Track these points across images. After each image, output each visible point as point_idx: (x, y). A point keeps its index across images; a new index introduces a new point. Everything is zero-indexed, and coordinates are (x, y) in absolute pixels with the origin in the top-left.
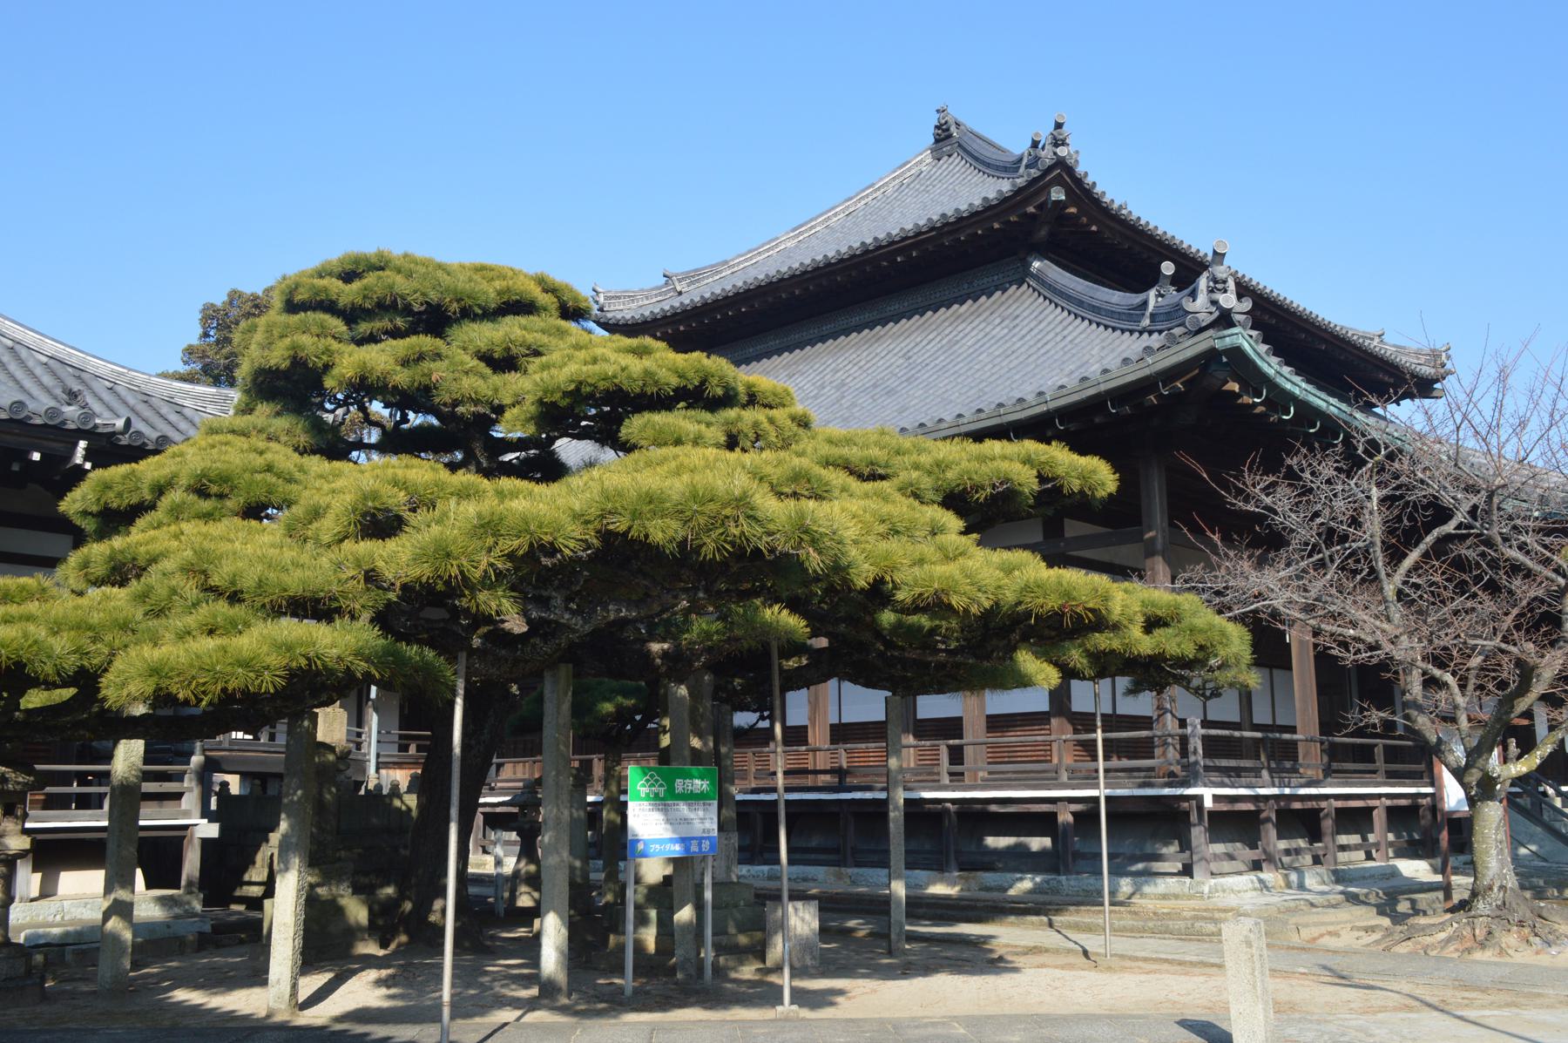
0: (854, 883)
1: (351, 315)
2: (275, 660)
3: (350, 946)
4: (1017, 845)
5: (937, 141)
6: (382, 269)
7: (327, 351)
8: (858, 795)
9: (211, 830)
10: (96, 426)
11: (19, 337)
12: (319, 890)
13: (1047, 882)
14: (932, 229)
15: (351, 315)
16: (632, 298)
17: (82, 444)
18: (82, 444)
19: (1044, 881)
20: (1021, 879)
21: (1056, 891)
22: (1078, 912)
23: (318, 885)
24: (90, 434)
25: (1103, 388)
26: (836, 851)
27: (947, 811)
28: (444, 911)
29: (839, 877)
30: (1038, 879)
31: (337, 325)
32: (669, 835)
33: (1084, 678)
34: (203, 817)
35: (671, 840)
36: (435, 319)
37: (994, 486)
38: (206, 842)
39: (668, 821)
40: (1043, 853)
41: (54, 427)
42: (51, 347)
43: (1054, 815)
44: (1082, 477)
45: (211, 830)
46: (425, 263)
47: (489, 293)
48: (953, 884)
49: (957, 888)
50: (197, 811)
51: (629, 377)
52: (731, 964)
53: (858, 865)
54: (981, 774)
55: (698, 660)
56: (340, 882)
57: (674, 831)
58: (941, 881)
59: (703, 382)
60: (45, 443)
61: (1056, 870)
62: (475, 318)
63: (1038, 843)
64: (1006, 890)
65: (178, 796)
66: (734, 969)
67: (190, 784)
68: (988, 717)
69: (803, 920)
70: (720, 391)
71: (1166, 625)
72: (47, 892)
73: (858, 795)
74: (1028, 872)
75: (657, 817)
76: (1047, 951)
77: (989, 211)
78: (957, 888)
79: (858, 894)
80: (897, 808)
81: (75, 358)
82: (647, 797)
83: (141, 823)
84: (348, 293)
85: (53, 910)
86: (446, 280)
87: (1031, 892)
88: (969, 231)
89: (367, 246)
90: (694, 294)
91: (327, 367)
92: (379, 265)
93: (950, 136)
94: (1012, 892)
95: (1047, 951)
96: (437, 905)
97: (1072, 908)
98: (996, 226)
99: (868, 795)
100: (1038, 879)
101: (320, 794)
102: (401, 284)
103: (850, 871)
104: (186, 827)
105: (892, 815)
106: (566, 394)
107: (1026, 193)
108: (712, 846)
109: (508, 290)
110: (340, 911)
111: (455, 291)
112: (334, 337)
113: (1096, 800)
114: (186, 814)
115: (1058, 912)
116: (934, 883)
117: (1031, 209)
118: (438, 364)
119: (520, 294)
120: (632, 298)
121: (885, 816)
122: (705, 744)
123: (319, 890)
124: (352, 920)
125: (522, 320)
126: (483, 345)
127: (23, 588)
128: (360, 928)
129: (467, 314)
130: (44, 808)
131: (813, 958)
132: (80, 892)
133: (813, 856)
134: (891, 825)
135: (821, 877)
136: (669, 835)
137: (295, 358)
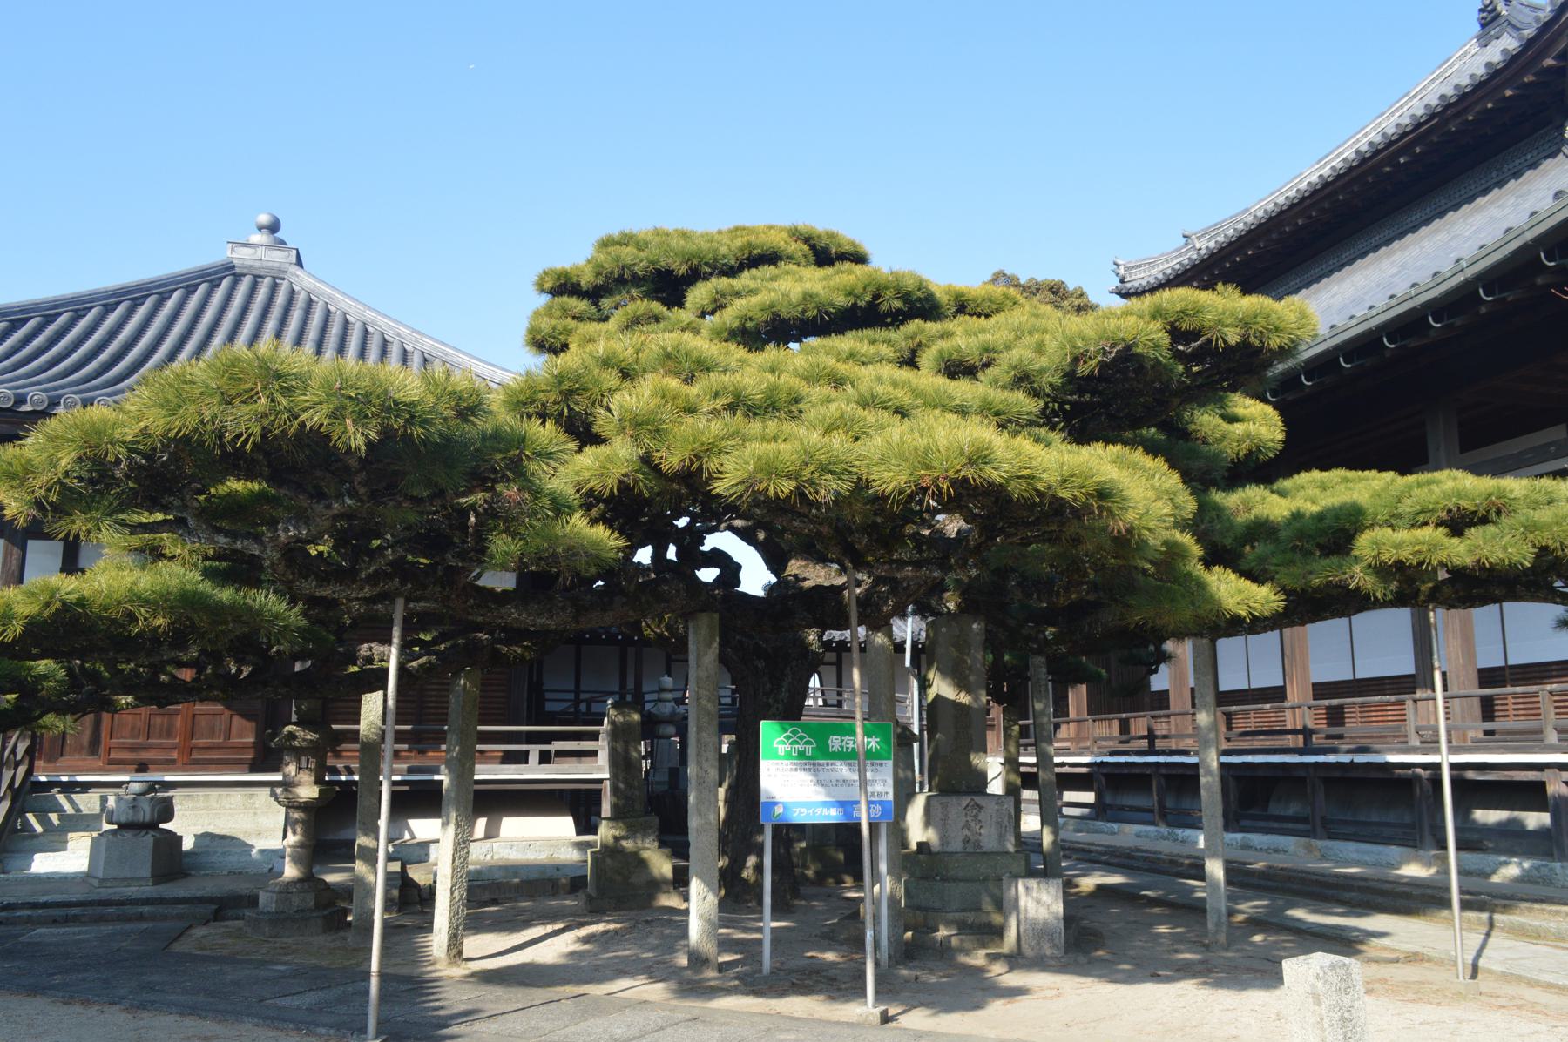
0: (1324, 858)
1: (594, 294)
3: (652, 897)
4: (1510, 821)
5: (1483, 26)
8: (1321, 758)
12: (624, 843)
13: (1538, 869)
14: (1432, 116)
16: (1152, 264)
19: (1534, 868)
20: (1506, 863)
21: (1548, 881)
22: (1530, 910)
25: (1529, 236)
26: (1305, 820)
27: (1418, 777)
28: (759, 868)
29: (1309, 849)
30: (1526, 865)
31: (582, 305)
33: (1377, 604)
35: (825, 804)
36: (668, 285)
37: (1105, 353)
39: (820, 783)
40: (1542, 833)
43: (1541, 786)
44: (1245, 324)
46: (657, 232)
47: (728, 250)
48: (1429, 865)
49: (1433, 870)
52: (967, 945)
53: (1331, 837)
54: (1471, 734)
55: (886, 603)
56: (645, 836)
57: (828, 794)
58: (1416, 859)
59: (876, 296)
61: (1549, 855)
63: (1535, 820)
64: (1488, 876)
65: (594, 753)
66: (967, 952)
67: (603, 746)
68: (1481, 671)
69: (1038, 902)
70: (897, 304)
71: (1484, 521)
72: (491, 834)
73: (1321, 758)
74: (1513, 853)
75: (805, 778)
76: (1430, 960)
77: (1496, 77)
78: (1433, 870)
79: (1345, 876)
80: (1209, 772)
82: (789, 755)
83: (476, 777)
85: (484, 850)
87: (1518, 880)
88: (1478, 108)
90: (1206, 245)
92: (626, 240)
93: (1498, 16)
94: (1495, 879)
95: (1430, 960)
96: (751, 861)
97: (1524, 905)
98: (1508, 93)
99: (1331, 758)
100: (1526, 865)
101: (627, 751)
103: (1319, 843)
105: (1203, 780)
107: (1538, 44)
108: (884, 812)
109: (750, 244)
110: (643, 864)
113: (1436, 767)
115: (1506, 909)
116: (1408, 861)
117: (1549, 62)
120: (1152, 264)
121: (1195, 778)
122: (976, 699)
123: (624, 843)
124: (656, 873)
128: (665, 881)
131: (1056, 946)
133: (1290, 826)
134: (1203, 792)
135: (1291, 849)
136: (823, 798)
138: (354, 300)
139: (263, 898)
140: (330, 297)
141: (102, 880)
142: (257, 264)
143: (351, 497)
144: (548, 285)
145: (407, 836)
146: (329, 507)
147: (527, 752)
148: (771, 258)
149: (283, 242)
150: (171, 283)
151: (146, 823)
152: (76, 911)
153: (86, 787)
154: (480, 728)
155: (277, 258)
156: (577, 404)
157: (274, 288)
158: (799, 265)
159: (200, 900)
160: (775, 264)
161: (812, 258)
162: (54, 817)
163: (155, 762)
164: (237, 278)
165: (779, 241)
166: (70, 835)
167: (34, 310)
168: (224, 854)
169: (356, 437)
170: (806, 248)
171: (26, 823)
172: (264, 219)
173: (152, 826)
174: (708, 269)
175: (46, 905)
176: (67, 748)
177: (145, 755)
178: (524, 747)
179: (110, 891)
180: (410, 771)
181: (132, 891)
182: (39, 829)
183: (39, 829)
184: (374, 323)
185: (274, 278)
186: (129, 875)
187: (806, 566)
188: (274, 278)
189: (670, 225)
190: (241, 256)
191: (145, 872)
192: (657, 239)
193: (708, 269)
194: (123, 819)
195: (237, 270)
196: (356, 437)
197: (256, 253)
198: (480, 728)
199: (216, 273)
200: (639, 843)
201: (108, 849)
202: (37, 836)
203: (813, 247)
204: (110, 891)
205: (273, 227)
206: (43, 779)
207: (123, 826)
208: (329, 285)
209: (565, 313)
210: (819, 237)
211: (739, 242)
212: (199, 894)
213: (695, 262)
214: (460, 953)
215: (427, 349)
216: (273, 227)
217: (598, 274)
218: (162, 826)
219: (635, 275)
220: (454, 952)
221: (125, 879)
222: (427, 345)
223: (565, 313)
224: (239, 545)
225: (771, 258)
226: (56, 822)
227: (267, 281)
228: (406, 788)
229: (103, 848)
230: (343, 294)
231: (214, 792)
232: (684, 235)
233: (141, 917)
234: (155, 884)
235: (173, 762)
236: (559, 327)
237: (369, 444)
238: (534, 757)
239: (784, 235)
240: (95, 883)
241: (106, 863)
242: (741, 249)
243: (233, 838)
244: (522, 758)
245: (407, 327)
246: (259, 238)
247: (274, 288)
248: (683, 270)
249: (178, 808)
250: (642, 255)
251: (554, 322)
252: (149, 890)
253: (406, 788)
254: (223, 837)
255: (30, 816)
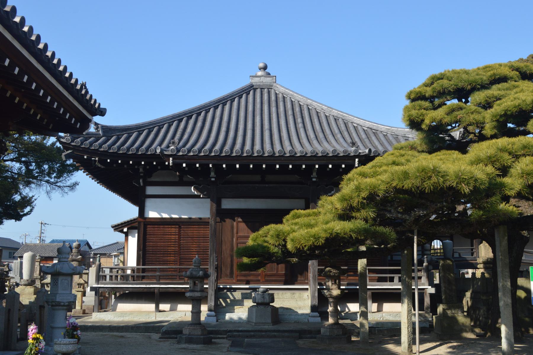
1: (431, 99)
2: (324, 235)
6: (442, 79)
7: (423, 115)
9: (432, 290)
10: (360, 153)
11: (358, 122)
15: (431, 99)
17: (357, 160)
18: (357, 160)
23: (447, 309)
24: (358, 156)
31: (427, 104)
32: (332, 291)
34: (429, 286)
36: (462, 93)
38: (431, 295)
41: (346, 156)
42: (368, 124)
45: (432, 290)
46: (454, 72)
47: (485, 77)
50: (427, 283)
51: (526, 104)
60: (346, 161)
62: (478, 90)
72: (380, 310)
81: (375, 126)
83: (368, 287)
84: (429, 91)
85: (380, 316)
86: (464, 76)
89: (437, 71)
91: (423, 120)
92: (441, 77)
102: (445, 82)
104: (424, 289)
106: (501, 116)
111: (468, 81)
112: (424, 109)
114: (423, 284)
118: (461, 112)
119: (499, 75)
125: (500, 86)
126: (478, 101)
127: (314, 213)
129: (474, 89)
130: (378, 282)
132: (391, 310)
137: (410, 119)
138: (302, 96)
139: (322, 330)
140: (292, 95)
141: (255, 323)
142: (261, 84)
143: (446, 202)
144: (413, 96)
145: (347, 310)
146: (437, 205)
147: (394, 277)
148: (503, 79)
149: (269, 74)
150: (234, 95)
151: (265, 303)
152: (252, 333)
153: (235, 290)
154: (400, 268)
155: (268, 80)
156: (496, 164)
157: (269, 93)
158: (515, 81)
159: (292, 331)
160: (506, 82)
161: (520, 77)
162: (228, 300)
163: (252, 281)
164: (255, 90)
165: (506, 71)
166: (236, 307)
167: (194, 112)
168: (290, 315)
169: (466, 189)
170: (518, 73)
171: (220, 302)
172: (261, 65)
173: (268, 304)
174: (479, 87)
175: (241, 331)
176: (222, 275)
177: (249, 278)
178: (392, 275)
179: (260, 327)
180: (348, 284)
181: (266, 327)
182: (224, 305)
183: (224, 305)
184: (311, 105)
185: (268, 89)
186: (264, 322)
187: (519, 201)
188: (268, 89)
189: (462, 68)
190: (255, 81)
191: (269, 321)
192: (456, 75)
193: (479, 87)
194: (260, 301)
195: (255, 87)
196: (466, 189)
197: (261, 80)
198: (400, 268)
199: (248, 89)
200: (453, 312)
201: (256, 312)
202: (224, 307)
203: (520, 72)
204: (260, 327)
205: (265, 68)
206: (221, 286)
207: (258, 304)
208: (291, 91)
209: (421, 108)
210: (522, 68)
211: (489, 74)
212: (291, 329)
213: (474, 84)
214: (412, 351)
215: (335, 114)
216: (265, 68)
217: (433, 92)
218: (271, 304)
219: (450, 91)
220: (410, 350)
221: (263, 323)
222: (335, 113)
223: (421, 108)
224: (404, 217)
225: (503, 79)
226: (229, 302)
227: (266, 90)
228: (347, 291)
229: (254, 312)
230: (297, 93)
231: (297, 293)
232: (466, 72)
233: (275, 337)
234: (273, 325)
235: (259, 280)
236: (420, 114)
237: (471, 191)
238: (396, 280)
239: (507, 68)
240: (253, 324)
241: (256, 317)
242: (491, 76)
243: (290, 309)
244: (392, 280)
245: (325, 106)
246: (260, 73)
247: (269, 93)
248: (469, 87)
249: (275, 297)
250: (451, 83)
251: (417, 111)
252: (271, 327)
253: (347, 291)
254: (287, 309)
255: (221, 300)
